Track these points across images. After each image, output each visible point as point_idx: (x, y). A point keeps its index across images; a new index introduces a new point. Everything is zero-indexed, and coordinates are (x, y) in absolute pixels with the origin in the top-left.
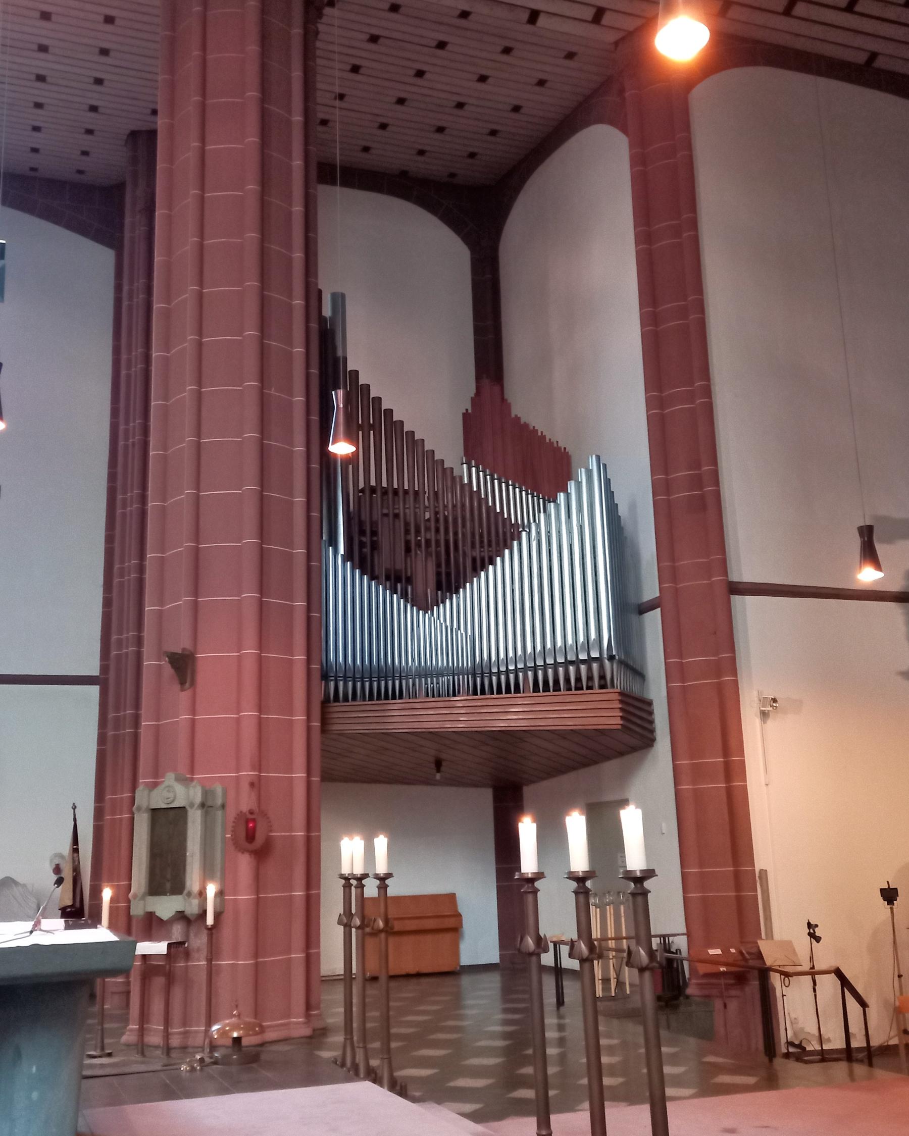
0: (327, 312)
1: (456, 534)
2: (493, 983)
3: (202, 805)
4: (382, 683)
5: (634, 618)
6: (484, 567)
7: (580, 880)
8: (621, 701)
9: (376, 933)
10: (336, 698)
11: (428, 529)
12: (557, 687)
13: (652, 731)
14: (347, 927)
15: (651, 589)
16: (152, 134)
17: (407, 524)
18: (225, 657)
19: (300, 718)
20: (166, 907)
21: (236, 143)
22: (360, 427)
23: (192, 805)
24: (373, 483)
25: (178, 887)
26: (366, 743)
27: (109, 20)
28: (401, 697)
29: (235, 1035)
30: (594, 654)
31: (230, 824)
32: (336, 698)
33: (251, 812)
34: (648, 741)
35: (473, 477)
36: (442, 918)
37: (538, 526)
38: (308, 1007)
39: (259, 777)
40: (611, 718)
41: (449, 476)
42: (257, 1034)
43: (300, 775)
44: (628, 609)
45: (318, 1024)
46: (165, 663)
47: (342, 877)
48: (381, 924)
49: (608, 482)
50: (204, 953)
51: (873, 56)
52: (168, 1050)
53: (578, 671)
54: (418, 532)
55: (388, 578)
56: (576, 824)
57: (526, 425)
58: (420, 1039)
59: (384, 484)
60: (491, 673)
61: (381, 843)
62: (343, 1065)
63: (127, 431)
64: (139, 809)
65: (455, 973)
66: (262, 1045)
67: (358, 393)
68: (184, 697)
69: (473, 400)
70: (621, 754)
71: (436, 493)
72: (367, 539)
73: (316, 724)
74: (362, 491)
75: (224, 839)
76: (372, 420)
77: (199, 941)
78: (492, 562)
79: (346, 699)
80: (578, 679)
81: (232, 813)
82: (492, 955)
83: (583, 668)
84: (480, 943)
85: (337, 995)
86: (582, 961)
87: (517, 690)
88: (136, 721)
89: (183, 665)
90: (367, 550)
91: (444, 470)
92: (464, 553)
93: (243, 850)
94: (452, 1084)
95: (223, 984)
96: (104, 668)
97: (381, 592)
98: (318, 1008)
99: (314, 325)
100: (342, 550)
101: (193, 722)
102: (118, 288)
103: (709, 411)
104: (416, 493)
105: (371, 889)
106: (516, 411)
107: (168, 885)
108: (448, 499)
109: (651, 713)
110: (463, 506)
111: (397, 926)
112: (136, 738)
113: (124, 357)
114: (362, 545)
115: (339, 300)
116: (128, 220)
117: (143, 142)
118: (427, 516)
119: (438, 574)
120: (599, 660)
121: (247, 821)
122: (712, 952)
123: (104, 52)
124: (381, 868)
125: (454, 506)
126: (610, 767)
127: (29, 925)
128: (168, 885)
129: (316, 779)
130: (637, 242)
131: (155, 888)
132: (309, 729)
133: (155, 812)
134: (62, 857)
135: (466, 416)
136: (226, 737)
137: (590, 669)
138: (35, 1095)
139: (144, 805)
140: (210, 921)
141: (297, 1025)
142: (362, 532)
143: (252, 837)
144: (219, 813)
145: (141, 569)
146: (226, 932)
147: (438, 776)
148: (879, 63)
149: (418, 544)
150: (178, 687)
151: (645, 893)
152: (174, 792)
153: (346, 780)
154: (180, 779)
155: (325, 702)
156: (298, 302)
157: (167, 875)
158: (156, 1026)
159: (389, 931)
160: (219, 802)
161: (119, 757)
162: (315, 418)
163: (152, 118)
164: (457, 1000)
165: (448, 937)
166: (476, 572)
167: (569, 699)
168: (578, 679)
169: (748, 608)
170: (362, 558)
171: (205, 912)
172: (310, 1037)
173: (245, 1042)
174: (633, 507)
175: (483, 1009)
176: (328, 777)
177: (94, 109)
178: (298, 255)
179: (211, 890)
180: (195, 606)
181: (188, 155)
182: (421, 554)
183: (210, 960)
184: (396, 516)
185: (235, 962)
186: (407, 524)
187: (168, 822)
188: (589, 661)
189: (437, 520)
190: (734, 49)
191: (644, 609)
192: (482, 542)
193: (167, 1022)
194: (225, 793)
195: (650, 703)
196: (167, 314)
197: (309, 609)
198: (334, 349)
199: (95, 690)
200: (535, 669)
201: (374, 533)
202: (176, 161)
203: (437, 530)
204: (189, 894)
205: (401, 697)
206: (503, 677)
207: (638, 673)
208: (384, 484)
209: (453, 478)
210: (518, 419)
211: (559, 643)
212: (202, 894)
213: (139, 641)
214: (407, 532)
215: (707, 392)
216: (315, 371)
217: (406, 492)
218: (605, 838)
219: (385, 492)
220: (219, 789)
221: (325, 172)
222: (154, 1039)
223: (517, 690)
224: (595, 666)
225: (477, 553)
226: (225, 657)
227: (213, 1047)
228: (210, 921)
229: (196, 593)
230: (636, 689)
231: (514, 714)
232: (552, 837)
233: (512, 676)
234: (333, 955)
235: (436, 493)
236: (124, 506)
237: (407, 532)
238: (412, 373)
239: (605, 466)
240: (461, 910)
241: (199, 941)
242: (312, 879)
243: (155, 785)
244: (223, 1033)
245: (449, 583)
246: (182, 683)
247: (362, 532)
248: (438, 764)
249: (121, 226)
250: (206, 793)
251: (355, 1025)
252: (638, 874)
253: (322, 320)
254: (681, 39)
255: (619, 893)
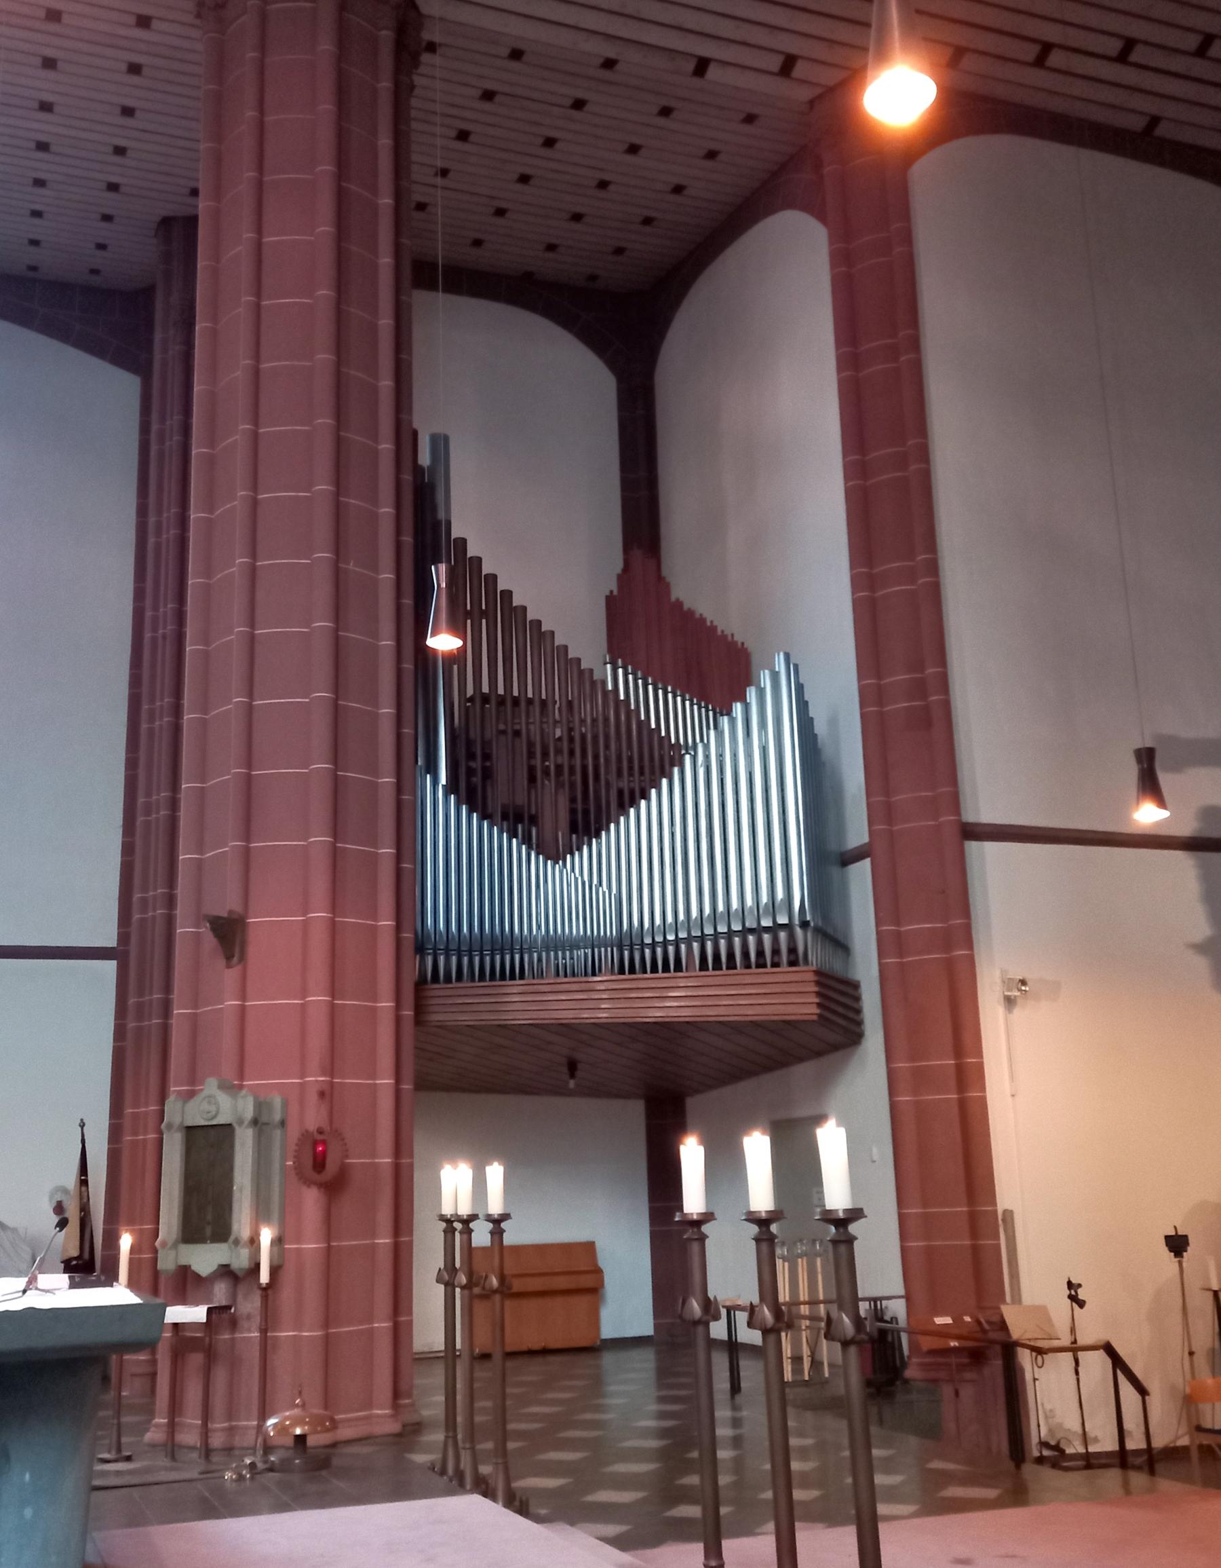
0: (425, 459)
1: (596, 757)
2: (644, 1363)
3: (255, 1122)
4: (497, 957)
5: (835, 871)
6: (634, 803)
7: (763, 1222)
8: (818, 983)
9: (487, 1295)
10: (435, 978)
11: (558, 751)
12: (731, 964)
13: (859, 1023)
14: (450, 1286)
15: (857, 833)
16: (191, 222)
17: (531, 745)
18: (287, 924)
19: (386, 1004)
20: (205, 1259)
21: (303, 235)
22: (468, 614)
23: (241, 1122)
24: (485, 689)
25: (222, 1233)
26: (479, 1037)
27: (135, 69)
28: (522, 977)
29: (298, 1431)
30: (783, 919)
31: (292, 1147)
32: (435, 978)
33: (320, 1131)
34: (853, 1036)
35: (620, 681)
36: (576, 1273)
37: (707, 747)
38: (397, 1394)
39: (332, 1084)
40: (802, 1004)
41: (587, 680)
42: (328, 1430)
43: (386, 1081)
44: (827, 859)
45: (410, 1418)
46: (205, 930)
47: (443, 1218)
48: (495, 1282)
49: (800, 688)
50: (257, 1320)
51: (1155, 121)
52: (207, 1452)
53: (760, 943)
54: (545, 755)
55: (505, 817)
56: (757, 1148)
57: (691, 613)
58: (548, 1436)
59: (501, 691)
60: (643, 945)
61: (495, 1173)
62: (443, 1472)
63: (155, 620)
64: (170, 1126)
65: (595, 1348)
66: (334, 1445)
67: (466, 569)
68: (231, 976)
69: (620, 577)
70: (819, 1054)
71: (570, 703)
72: (477, 764)
73: (408, 1013)
74: (471, 699)
75: (283, 1167)
76: (484, 604)
77: (249, 1305)
78: (645, 795)
79: (448, 979)
80: (760, 953)
81: (294, 1132)
82: (645, 1327)
83: (767, 937)
84: (628, 1307)
85: (437, 1377)
86: (766, 1332)
87: (678, 967)
88: (166, 1008)
89: (229, 934)
90: (477, 780)
91: (581, 672)
92: (608, 784)
93: (308, 1183)
94: (590, 1498)
95: (282, 1362)
96: (123, 937)
97: (496, 836)
98: (409, 1396)
99: (407, 477)
100: (443, 780)
101: (243, 1009)
102: (145, 428)
103: (935, 593)
104: (544, 703)
105: (481, 1236)
106: (680, 591)
107: (208, 1231)
108: (586, 711)
109: (858, 999)
110: (606, 720)
111: (517, 1285)
112: (165, 1030)
113: (152, 519)
114: (470, 772)
115: (440, 444)
116: (158, 336)
117: (178, 232)
118: (558, 733)
119: (573, 812)
120: (788, 927)
121: (316, 1143)
122: (939, 1320)
123: (128, 112)
124: (495, 1206)
125: (594, 721)
126: (803, 1071)
127: (22, 1282)
128: (208, 1231)
129: (407, 1086)
130: (840, 369)
131: (191, 1233)
132: (398, 1020)
133: (190, 1130)
134: (65, 1191)
135: (610, 600)
136: (288, 1030)
137: (775, 940)
138: (28, 1512)
139: (177, 1121)
140: (264, 1277)
141: (381, 1418)
142: (471, 756)
143: (321, 1166)
144: (278, 1134)
145: (174, 804)
146: (286, 1294)
147: (572, 1084)
148: (1161, 131)
149: (546, 772)
150: (221, 962)
151: (850, 1241)
152: (216, 1103)
153: (448, 1088)
154: (223, 1087)
155: (421, 984)
156: (386, 446)
157: (207, 1216)
158: (192, 1420)
159: (506, 1291)
160: (277, 1117)
161: (143, 1056)
162: (408, 601)
163: (191, 200)
164: (596, 1385)
165: (582, 1302)
166: (623, 809)
167: (748, 980)
168: (760, 953)
169: (989, 860)
170: (471, 790)
171: (258, 1266)
172: (399, 1435)
173: (311, 1441)
174: (833, 722)
175: (631, 1398)
176: (424, 1084)
177: (113, 187)
178: (386, 383)
179: (266, 1236)
180: (247, 854)
181: (239, 249)
182: (550, 785)
183: (264, 1331)
184: (517, 733)
185: (298, 1333)
186: (531, 745)
187: (207, 1145)
188: (775, 929)
189: (571, 740)
190: (967, 112)
191: (848, 859)
192: (631, 768)
193: (206, 1416)
194: (285, 1105)
195: (856, 986)
196: (210, 462)
197: (399, 858)
198: (434, 509)
199: (111, 966)
200: (702, 939)
201: (487, 757)
202: (223, 257)
203: (572, 753)
204: (237, 1242)
205: (522, 977)
206: (659, 950)
207: (840, 945)
208: (501, 691)
209: (593, 683)
210: (679, 604)
211: (735, 904)
212: (254, 1241)
213: (171, 901)
214: (531, 754)
215: (933, 568)
216: (408, 539)
217: (530, 702)
218: (797, 1166)
219: (501, 701)
220: (277, 1101)
221: (423, 273)
222: (189, 1437)
223: (678, 967)
224: (783, 935)
225: (624, 784)
226: (287, 924)
227: (268, 1449)
228: (264, 1277)
229: (247, 836)
230: (837, 966)
231: (675, 1000)
232: (725, 1165)
233: (671, 949)
234: (430, 1323)
235: (570, 703)
236: (151, 719)
237: (531, 754)
238: (536, 538)
239: (796, 667)
240: (602, 1263)
241: (249, 1305)
242: (401, 1222)
243: (191, 1094)
244: (281, 1429)
245: (587, 824)
246: (229, 957)
247: (471, 756)
248: (572, 1067)
249: (150, 342)
250: (259, 1106)
251: (459, 1419)
252: (841, 1215)
253: (417, 470)
254: (899, 95)
255: (814, 1241)
